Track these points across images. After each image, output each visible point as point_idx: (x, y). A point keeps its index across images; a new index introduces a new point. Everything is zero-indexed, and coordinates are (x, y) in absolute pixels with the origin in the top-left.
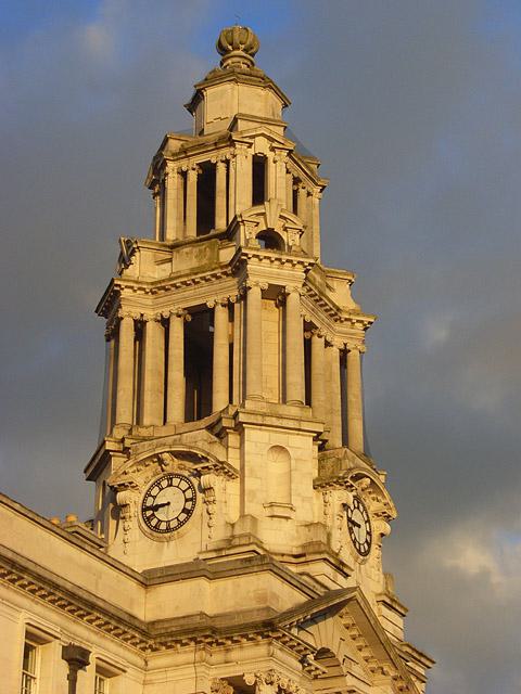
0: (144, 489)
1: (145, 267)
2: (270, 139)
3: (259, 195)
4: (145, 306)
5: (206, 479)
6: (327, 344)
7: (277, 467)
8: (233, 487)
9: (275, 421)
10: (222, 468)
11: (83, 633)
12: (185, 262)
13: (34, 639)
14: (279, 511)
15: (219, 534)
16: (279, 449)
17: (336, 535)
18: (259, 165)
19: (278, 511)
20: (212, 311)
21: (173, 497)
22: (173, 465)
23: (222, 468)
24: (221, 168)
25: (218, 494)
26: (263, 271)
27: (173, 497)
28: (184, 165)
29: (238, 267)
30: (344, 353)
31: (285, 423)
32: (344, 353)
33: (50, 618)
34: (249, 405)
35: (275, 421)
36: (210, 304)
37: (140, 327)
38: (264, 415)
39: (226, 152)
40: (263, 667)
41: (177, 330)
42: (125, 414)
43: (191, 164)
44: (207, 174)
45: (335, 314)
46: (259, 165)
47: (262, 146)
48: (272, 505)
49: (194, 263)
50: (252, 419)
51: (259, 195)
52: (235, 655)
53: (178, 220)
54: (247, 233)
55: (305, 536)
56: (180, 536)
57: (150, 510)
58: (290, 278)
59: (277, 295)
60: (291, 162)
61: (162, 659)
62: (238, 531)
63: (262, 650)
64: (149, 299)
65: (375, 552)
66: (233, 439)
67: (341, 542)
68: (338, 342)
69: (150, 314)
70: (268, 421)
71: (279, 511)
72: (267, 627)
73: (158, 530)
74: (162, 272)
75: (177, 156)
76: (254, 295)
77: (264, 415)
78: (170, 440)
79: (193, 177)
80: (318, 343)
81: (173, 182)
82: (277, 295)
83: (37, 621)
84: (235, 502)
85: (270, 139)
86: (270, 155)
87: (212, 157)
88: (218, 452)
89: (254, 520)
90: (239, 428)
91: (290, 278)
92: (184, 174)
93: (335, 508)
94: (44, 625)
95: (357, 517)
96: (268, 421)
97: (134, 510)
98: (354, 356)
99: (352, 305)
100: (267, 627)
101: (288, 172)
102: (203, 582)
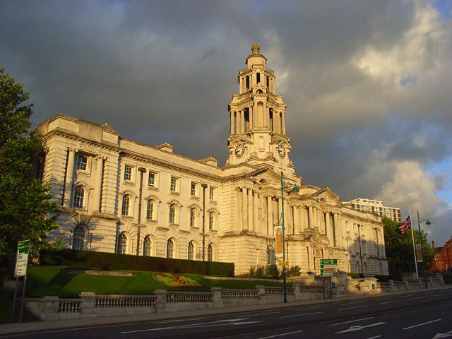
1: (236, 100)
3: (258, 81)
5: (245, 146)
7: (261, 141)
10: (249, 142)
11: (206, 181)
12: (243, 98)
14: (262, 150)
15: (249, 156)
18: (258, 75)
22: (240, 143)
23: (249, 142)
24: (250, 109)
26: (257, 99)
27: (240, 149)
28: (243, 77)
29: (252, 98)
30: (281, 114)
32: (281, 114)
37: (235, 113)
39: (251, 73)
40: (243, 185)
41: (243, 113)
42: (233, 132)
43: (244, 77)
44: (248, 77)
45: (278, 105)
46: (258, 75)
47: (258, 71)
51: (258, 81)
53: (242, 88)
54: (254, 91)
55: (268, 155)
57: (236, 153)
59: (260, 103)
61: (226, 184)
63: (243, 181)
64: (237, 107)
65: (287, 156)
66: (252, 136)
67: (277, 156)
69: (237, 110)
71: (262, 150)
72: (244, 177)
73: (238, 157)
75: (241, 75)
76: (256, 104)
80: (274, 112)
81: (241, 80)
83: (152, 169)
87: (248, 75)
90: (253, 134)
91: (264, 99)
94: (196, 181)
95: (281, 149)
97: (234, 152)
98: (283, 114)
99: (282, 103)
100: (244, 177)
102: (233, 169)
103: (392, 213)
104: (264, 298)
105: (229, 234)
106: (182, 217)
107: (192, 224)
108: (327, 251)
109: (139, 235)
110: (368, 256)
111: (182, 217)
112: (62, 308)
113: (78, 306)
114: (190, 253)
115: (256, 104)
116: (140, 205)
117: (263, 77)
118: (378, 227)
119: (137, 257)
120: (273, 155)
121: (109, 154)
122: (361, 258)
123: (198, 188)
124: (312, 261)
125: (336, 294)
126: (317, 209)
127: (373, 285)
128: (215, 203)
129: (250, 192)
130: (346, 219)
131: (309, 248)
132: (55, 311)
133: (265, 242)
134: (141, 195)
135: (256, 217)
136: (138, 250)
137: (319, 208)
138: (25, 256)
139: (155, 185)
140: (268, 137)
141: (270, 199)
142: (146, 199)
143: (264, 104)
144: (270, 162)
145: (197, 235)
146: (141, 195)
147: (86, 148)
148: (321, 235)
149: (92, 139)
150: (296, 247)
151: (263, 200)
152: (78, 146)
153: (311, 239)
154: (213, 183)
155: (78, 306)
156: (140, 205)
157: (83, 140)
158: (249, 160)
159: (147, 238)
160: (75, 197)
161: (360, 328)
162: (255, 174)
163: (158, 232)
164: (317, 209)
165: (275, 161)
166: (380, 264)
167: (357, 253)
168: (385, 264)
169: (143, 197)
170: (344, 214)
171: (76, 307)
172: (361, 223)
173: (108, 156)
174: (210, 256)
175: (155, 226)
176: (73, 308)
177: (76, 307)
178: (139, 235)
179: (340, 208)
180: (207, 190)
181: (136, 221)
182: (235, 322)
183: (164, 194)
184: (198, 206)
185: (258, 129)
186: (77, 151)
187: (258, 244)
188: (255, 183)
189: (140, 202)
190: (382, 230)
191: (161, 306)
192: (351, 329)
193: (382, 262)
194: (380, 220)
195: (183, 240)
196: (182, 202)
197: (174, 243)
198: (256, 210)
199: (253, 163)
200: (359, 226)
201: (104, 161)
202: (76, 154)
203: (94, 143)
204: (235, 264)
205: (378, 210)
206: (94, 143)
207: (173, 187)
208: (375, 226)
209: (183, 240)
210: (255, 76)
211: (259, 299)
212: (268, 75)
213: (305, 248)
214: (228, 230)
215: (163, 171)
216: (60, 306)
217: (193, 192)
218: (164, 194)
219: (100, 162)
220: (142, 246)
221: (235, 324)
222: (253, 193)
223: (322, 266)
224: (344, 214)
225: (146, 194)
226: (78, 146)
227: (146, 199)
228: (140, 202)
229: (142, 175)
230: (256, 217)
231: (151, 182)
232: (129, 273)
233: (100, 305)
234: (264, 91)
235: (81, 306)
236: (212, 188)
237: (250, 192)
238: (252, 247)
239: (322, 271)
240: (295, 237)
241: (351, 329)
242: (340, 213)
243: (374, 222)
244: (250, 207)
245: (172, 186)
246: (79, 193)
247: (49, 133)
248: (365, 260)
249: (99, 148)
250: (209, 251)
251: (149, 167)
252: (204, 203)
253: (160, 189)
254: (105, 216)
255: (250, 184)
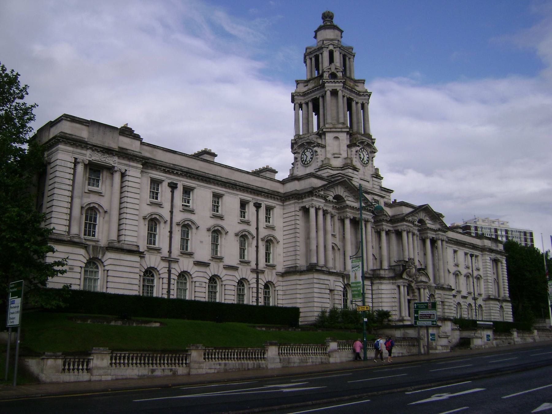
0: (301, 153)
2: (333, 45)
3: (331, 60)
4: (301, 100)
6: (357, 103)
7: (336, 143)
8: (323, 150)
9: (334, 130)
10: (319, 145)
13: (243, 204)
14: (336, 156)
15: (320, 164)
16: (336, 138)
17: (354, 160)
18: (331, 53)
19: (336, 156)
20: (319, 98)
21: (308, 154)
25: (319, 153)
26: (329, 86)
29: (323, 86)
31: (337, 130)
33: (247, 197)
34: (327, 126)
35: (334, 130)
36: (338, 90)
38: (331, 128)
46: (331, 53)
47: (331, 47)
48: (334, 154)
49: (313, 85)
50: (327, 130)
51: (331, 60)
52: (304, 200)
54: (326, 75)
56: (310, 165)
58: (338, 86)
59: (334, 93)
60: (341, 51)
62: (324, 163)
63: (310, 198)
66: (323, 137)
68: (360, 102)
69: (303, 102)
70: (332, 130)
71: (336, 156)
74: (305, 89)
76: (328, 93)
77: (331, 128)
78: (306, 139)
79: (313, 59)
82: (334, 93)
83: (243, 197)
84: (324, 154)
85: (333, 45)
86: (334, 50)
88: (319, 141)
89: (329, 159)
91: (338, 86)
92: (311, 59)
93: (354, 152)
96: (332, 130)
101: (340, 53)
103: (523, 237)
104: (336, 355)
105: (292, 269)
106: (229, 249)
107: (242, 255)
108: (427, 291)
109: (169, 272)
110: (484, 296)
111: (229, 249)
112: (67, 367)
113: (87, 365)
114: (241, 295)
115: (328, 93)
116: (171, 232)
117: (337, 56)
118: (499, 257)
119: (257, 307)
120: (352, 161)
121: (130, 166)
122: (475, 299)
123: (251, 210)
124: (405, 305)
125: (436, 349)
126: (413, 234)
127: (488, 336)
128: (273, 228)
129: (321, 213)
130: (455, 247)
131: (402, 288)
132: (58, 371)
133: (341, 280)
134: (171, 218)
135: (330, 247)
136: (257, 300)
137: (416, 232)
138: (18, 301)
139: (190, 204)
140: (344, 138)
141: (347, 222)
142: (178, 224)
143: (340, 93)
144: (349, 172)
145: (249, 272)
146: (171, 218)
147: (97, 157)
148: (419, 270)
149: (106, 145)
150: (384, 287)
151: (338, 224)
152: (88, 156)
153: (405, 276)
154: (271, 202)
155: (87, 365)
156: (171, 232)
157: (95, 148)
158: (320, 169)
159: (266, 286)
160: (86, 223)
161: (446, 396)
162: (324, 188)
163: (196, 268)
164: (413, 234)
165: (355, 169)
166: (501, 307)
167: (470, 293)
168: (508, 307)
169: (261, 236)
170: (451, 241)
171: (85, 367)
172: (476, 253)
173: (127, 168)
174: (267, 298)
175: (191, 261)
176: (81, 367)
177: (85, 367)
178: (169, 272)
179: (445, 232)
180: (262, 211)
181: (165, 253)
182: (287, 388)
183: (203, 217)
184: (249, 233)
185: (331, 126)
186: (87, 162)
187: (332, 282)
188: (326, 200)
189: (171, 228)
190: (504, 262)
191: (196, 366)
192: (434, 398)
193: (504, 304)
194: (501, 247)
195: (231, 278)
196: (198, 223)
197: (218, 282)
198: (329, 236)
199: (325, 173)
200: (472, 256)
201: (123, 175)
202: (86, 166)
203: (108, 151)
204: (301, 310)
205: (504, 233)
206: (108, 151)
207: (216, 207)
208: (493, 256)
209: (231, 278)
210: (326, 54)
211: (330, 356)
212: (344, 53)
213: (394, 287)
214: (290, 263)
215: (200, 186)
216: (64, 365)
217: (243, 213)
218: (203, 217)
219: (117, 177)
220: (261, 295)
221: (285, 390)
222: (324, 215)
223: (416, 312)
224: (451, 241)
225: (179, 216)
226: (88, 156)
227: (178, 224)
228: (171, 228)
229: (172, 192)
230: (330, 247)
231: (268, 219)
232: (156, 322)
233: (115, 363)
234: (340, 74)
235: (91, 365)
236: (269, 209)
237: (321, 213)
238: (324, 286)
239: (416, 318)
240: (382, 273)
241: (434, 398)
242: (445, 238)
243: (491, 251)
244: (321, 233)
245: (266, 217)
246: (91, 217)
247: (50, 140)
248: (480, 302)
249: (116, 159)
250: (265, 293)
251: (182, 182)
252: (257, 229)
253: (225, 218)
254: (125, 247)
255: (318, 202)
